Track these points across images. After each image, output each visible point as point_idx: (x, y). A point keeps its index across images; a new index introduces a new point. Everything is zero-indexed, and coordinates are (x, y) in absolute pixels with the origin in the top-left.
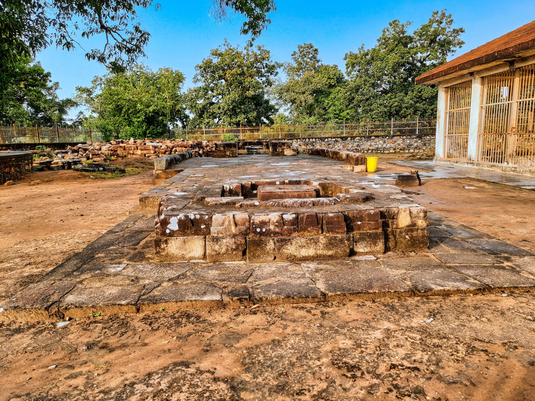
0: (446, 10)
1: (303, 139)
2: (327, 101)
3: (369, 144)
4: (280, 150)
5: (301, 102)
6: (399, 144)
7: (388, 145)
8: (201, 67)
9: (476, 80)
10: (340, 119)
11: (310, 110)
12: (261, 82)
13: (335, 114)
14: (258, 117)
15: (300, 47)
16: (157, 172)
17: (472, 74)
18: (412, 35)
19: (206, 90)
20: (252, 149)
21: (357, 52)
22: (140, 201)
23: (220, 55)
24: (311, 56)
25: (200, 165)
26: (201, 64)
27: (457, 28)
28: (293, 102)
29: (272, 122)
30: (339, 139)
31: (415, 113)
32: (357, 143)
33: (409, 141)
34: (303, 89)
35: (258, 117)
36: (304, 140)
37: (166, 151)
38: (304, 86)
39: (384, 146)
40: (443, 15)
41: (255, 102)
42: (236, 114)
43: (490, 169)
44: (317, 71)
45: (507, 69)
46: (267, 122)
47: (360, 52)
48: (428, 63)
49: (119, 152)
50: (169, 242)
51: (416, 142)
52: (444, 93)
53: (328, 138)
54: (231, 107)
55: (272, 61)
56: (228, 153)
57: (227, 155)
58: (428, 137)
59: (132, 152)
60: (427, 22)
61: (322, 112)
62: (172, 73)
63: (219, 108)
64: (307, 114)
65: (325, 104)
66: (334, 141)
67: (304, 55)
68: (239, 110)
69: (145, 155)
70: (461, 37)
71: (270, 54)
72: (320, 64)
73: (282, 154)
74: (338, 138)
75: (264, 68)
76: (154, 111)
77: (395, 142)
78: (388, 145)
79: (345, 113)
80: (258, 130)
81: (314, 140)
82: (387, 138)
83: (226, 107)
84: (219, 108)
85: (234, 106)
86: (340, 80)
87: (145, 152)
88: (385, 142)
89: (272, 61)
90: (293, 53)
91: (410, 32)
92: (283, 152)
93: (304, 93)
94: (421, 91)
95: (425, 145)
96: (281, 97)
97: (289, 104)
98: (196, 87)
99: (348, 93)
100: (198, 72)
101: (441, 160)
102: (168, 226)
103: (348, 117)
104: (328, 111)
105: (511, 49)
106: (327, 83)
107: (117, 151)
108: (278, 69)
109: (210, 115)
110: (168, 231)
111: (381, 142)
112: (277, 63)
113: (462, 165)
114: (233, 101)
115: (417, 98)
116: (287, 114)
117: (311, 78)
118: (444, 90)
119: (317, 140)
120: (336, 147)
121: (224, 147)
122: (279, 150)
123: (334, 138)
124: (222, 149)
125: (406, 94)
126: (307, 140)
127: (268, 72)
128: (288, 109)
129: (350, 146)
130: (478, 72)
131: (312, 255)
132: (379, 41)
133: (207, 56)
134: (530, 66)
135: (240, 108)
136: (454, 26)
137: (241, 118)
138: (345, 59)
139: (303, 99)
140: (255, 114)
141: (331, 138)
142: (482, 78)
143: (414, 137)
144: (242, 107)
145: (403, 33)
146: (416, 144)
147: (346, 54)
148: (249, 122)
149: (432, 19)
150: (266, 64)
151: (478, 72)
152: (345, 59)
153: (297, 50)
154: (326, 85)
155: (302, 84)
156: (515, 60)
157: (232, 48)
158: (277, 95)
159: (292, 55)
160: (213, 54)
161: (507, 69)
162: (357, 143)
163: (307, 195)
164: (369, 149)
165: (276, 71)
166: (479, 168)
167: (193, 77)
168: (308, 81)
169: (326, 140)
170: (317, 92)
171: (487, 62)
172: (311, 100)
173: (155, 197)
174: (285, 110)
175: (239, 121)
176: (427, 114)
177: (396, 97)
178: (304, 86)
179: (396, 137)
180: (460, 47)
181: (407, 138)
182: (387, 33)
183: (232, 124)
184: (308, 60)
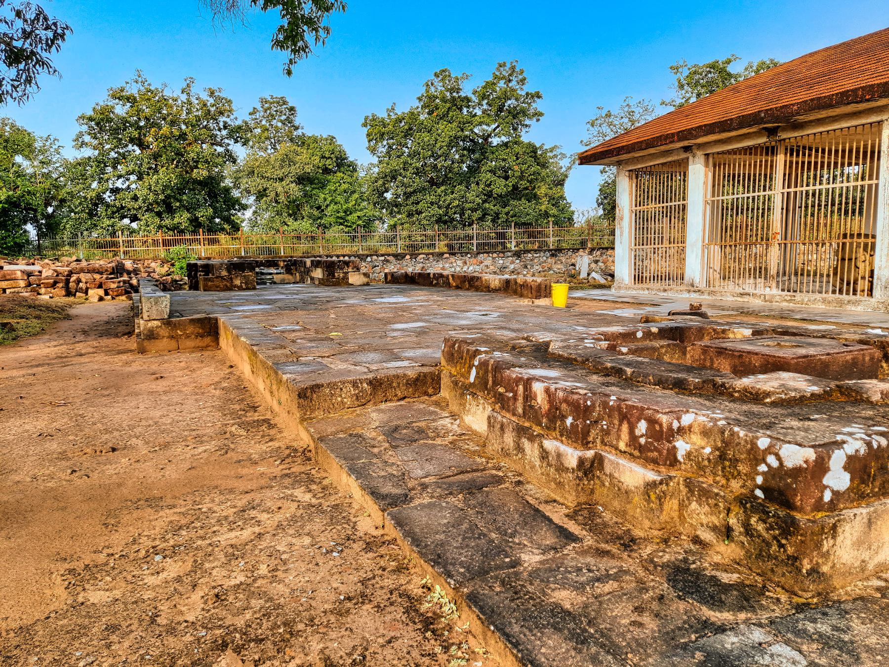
0: (517, 61)
2: (323, 196)
3: (441, 266)
5: (277, 195)
6: (487, 266)
7: (471, 268)
8: (91, 119)
9: (696, 159)
10: (347, 226)
11: (294, 209)
13: (338, 217)
15: (263, 101)
16: (150, 324)
17: (687, 149)
18: (470, 95)
19: (101, 163)
20: (262, 274)
21: (385, 115)
22: (300, 396)
23: (131, 100)
25: (493, 299)
26: (90, 113)
27: (532, 91)
30: (391, 258)
31: (482, 219)
32: (421, 265)
33: (501, 262)
37: (55, 283)
40: (513, 68)
42: (170, 210)
43: (739, 299)
44: (302, 142)
45: (762, 140)
47: (389, 115)
48: (495, 141)
50: (840, 530)
51: (513, 262)
52: (627, 179)
54: (161, 197)
55: (236, 119)
56: (237, 282)
57: (235, 286)
58: (530, 255)
60: (490, 79)
61: (316, 213)
63: (135, 198)
64: (290, 215)
65: (321, 200)
66: (383, 261)
70: (538, 105)
73: (344, 282)
74: (389, 255)
77: (482, 263)
78: (471, 268)
79: (355, 215)
82: (469, 256)
85: (168, 197)
86: (342, 162)
88: (465, 263)
89: (236, 119)
90: (252, 110)
91: (467, 90)
92: (345, 278)
93: (281, 180)
94: (490, 185)
95: (526, 267)
98: (79, 157)
99: (380, 182)
101: (628, 288)
102: (825, 481)
103: (360, 222)
104: (325, 212)
105: (795, 107)
109: (113, 213)
110: (827, 496)
111: (460, 263)
113: (676, 295)
114: (166, 187)
115: (485, 195)
117: (291, 156)
118: (627, 174)
121: (229, 270)
122: (339, 274)
124: (224, 273)
127: (230, 136)
130: (700, 146)
132: (420, 99)
133: (103, 99)
134: (812, 137)
135: (180, 201)
136: (529, 88)
137: (182, 218)
138: (365, 125)
139: (280, 189)
142: (707, 155)
143: (509, 254)
145: (458, 90)
146: (512, 267)
147: (366, 118)
149: (498, 73)
150: (225, 123)
151: (700, 146)
152: (365, 125)
153: (258, 106)
154: (318, 168)
155: (278, 164)
156: (779, 127)
159: (250, 114)
160: (114, 97)
161: (762, 140)
162: (421, 265)
166: (714, 297)
167: (74, 137)
168: (288, 160)
169: (369, 259)
171: (741, 126)
172: (295, 190)
173: (335, 384)
176: (500, 221)
177: (452, 193)
180: (538, 120)
181: (499, 257)
182: (433, 89)
184: (280, 124)
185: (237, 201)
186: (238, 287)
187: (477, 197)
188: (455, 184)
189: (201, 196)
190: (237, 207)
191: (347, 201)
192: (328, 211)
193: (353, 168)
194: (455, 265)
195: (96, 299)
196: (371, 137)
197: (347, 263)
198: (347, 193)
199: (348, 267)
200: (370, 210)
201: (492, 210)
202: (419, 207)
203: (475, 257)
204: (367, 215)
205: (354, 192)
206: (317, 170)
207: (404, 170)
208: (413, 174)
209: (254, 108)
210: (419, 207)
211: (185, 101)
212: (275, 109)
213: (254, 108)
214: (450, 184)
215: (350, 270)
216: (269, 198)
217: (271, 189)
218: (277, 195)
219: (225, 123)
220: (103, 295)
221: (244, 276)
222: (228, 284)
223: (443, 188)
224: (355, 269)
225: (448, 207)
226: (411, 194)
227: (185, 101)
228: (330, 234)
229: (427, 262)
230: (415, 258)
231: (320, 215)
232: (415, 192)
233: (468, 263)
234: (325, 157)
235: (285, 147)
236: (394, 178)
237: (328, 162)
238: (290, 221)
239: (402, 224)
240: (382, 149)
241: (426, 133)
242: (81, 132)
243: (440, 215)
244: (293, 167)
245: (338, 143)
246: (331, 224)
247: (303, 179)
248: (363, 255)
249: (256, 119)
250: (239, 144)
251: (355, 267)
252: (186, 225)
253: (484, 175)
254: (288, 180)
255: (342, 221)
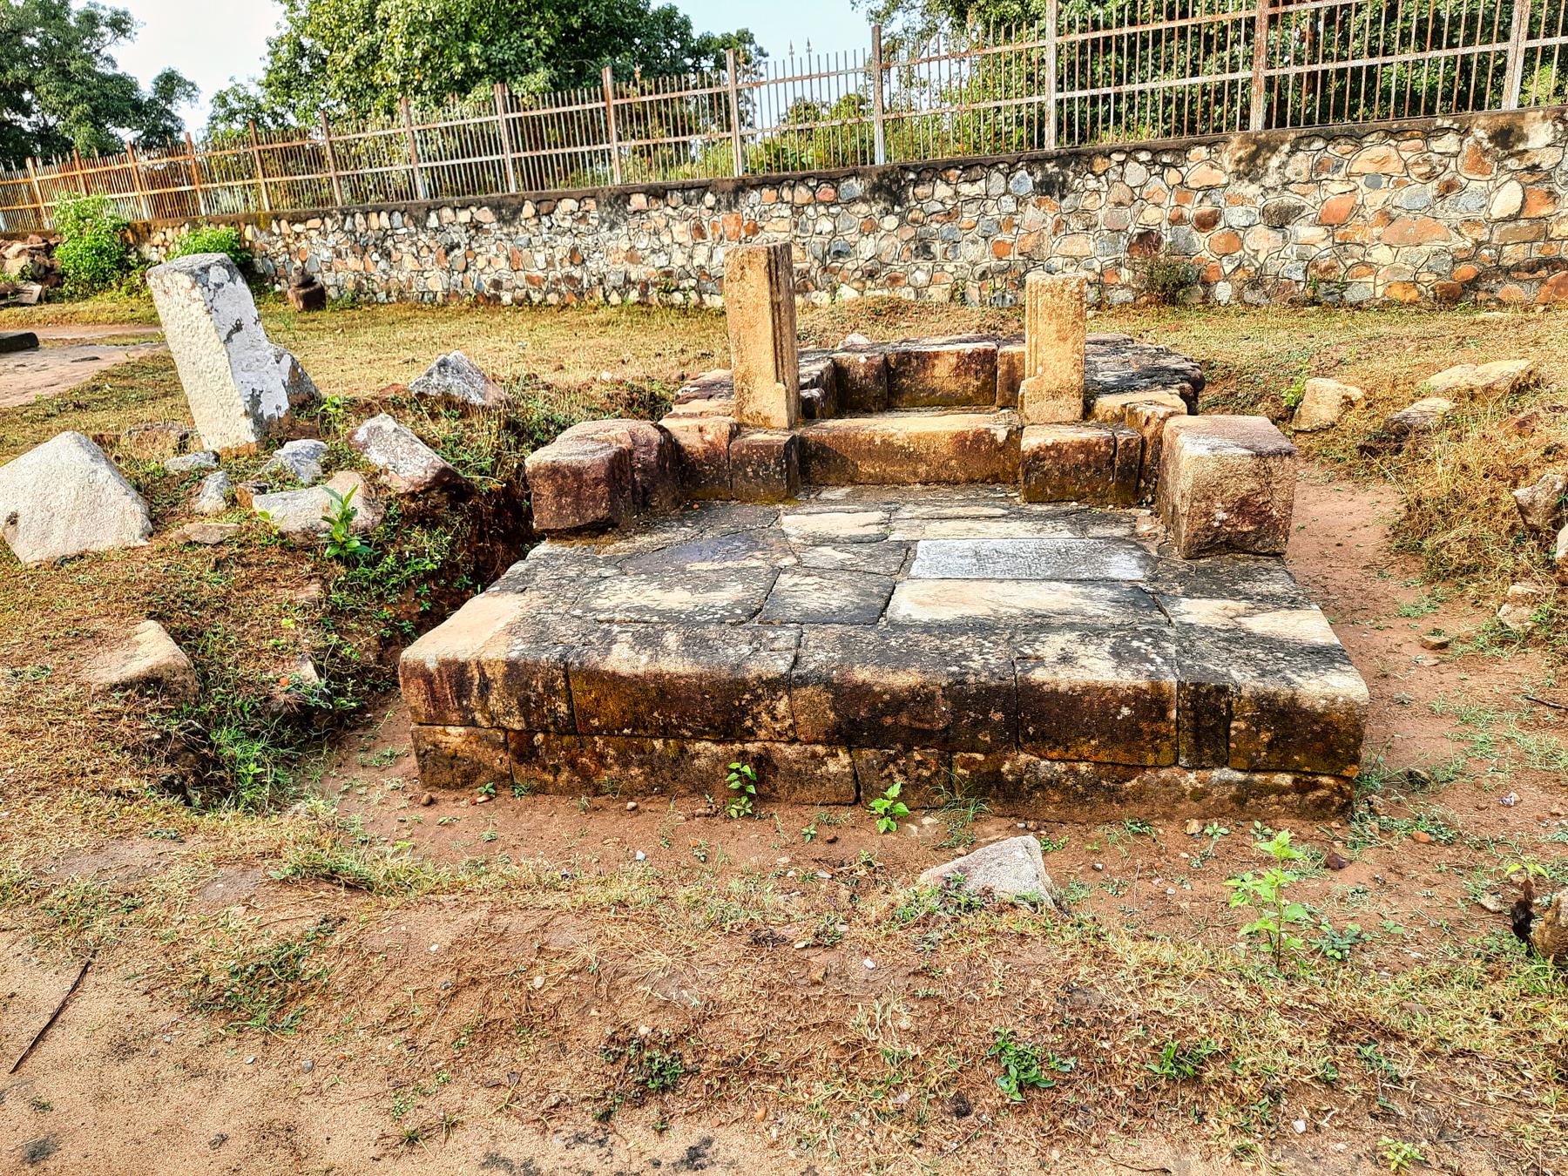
33: (826, 225)
51: (870, 228)
58: (942, 190)
62: (129, 126)
88: (699, 231)
95: (924, 249)
131: (624, 674)
146: (867, 247)
163: (408, 626)
179: (754, 196)
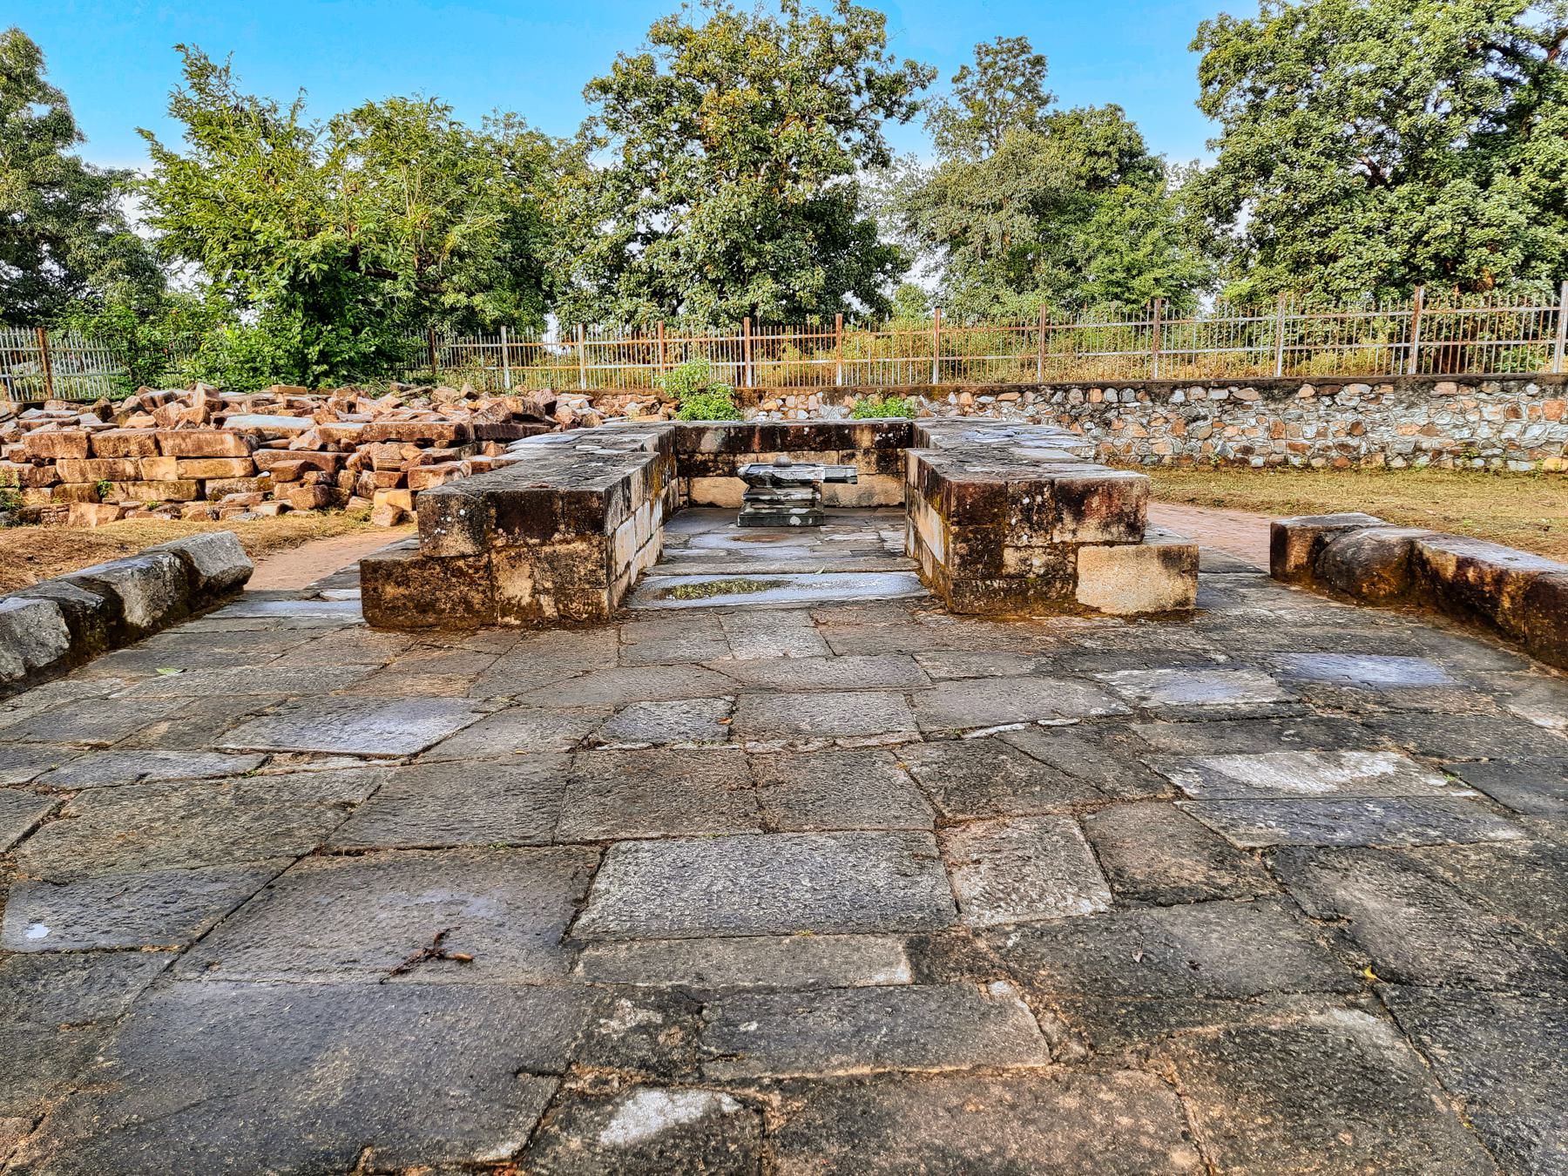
1: (1055, 388)
2: (1083, 237)
4: (1038, 561)
5: (987, 240)
8: (604, 88)
10: (1128, 301)
11: (1019, 269)
12: (846, 147)
13: (1111, 283)
14: (831, 291)
15: (983, 51)
20: (777, 483)
24: (1019, 81)
26: (607, 74)
28: (956, 240)
29: (882, 309)
30: (1250, 395)
34: (996, 194)
35: (831, 291)
36: (1059, 396)
38: (1001, 179)
39: (1512, 432)
41: (821, 230)
42: (741, 278)
44: (1057, 128)
46: (866, 310)
49: (61, 468)
53: (1186, 385)
54: (721, 247)
55: (891, 59)
56: (518, 586)
57: (508, 607)
59: (130, 469)
61: (1064, 275)
63: (676, 254)
64: (1009, 282)
66: (1222, 403)
67: (997, 79)
68: (753, 262)
69: (201, 483)
71: (887, 29)
72: (1049, 110)
74: (1243, 385)
75: (858, 93)
76: (326, 254)
78: (1536, 430)
79: (1148, 277)
80: (829, 344)
81: (1111, 395)
82: (1532, 388)
83: (701, 248)
84: (676, 254)
85: (735, 248)
87: (198, 468)
89: (891, 59)
90: (957, 73)
93: (998, 207)
96: (915, 225)
97: (942, 251)
99: (1226, 182)
100: (598, 109)
106: (1083, 170)
107: (52, 461)
108: (917, 90)
112: (913, 67)
114: (729, 224)
115: (1535, 202)
116: (931, 284)
119: (1128, 394)
120: (1229, 432)
121: (476, 527)
123: (1223, 386)
125: (1485, 185)
126: (1076, 395)
127: (878, 103)
128: (936, 269)
129: (1310, 431)
133: (636, 44)
135: (758, 254)
137: (762, 291)
139: (994, 228)
140: (819, 276)
141: (1206, 386)
144: (769, 246)
147: (1203, 27)
148: (796, 312)
150: (870, 73)
153: (972, 63)
154: (1079, 177)
157: (733, 14)
158: (898, 218)
162: (1350, 417)
164: (1418, 449)
165: (906, 99)
167: (578, 130)
168: (1015, 163)
169: (1178, 396)
170: (1043, 206)
172: (1024, 227)
174: (926, 274)
175: (754, 307)
178: (1001, 179)
183: (724, 318)
184: (1010, 96)
185: (889, 252)
186: (521, 611)
187: (1512, 207)
188: (1442, 176)
189: (805, 242)
190: (889, 267)
191: (1134, 246)
192: (1091, 271)
193: (1154, 172)
194: (1472, 418)
195: (387, 517)
196: (1211, 75)
197: (1073, 499)
198: (1136, 229)
199: (1079, 516)
200: (1186, 260)
201: (1554, 244)
202: (1330, 244)
203: (1555, 394)
204: (1177, 275)
205: (1152, 225)
206: (1075, 182)
207: (1296, 145)
208: (1321, 153)
209: (963, 68)
210: (1330, 244)
211: (787, 27)
212: (1003, 64)
213: (963, 68)
214: (1426, 177)
215: (1083, 535)
216: (971, 248)
217: (975, 229)
218: (987, 240)
219: (870, 73)
220: (408, 508)
221: (552, 559)
222: (476, 598)
223: (1404, 189)
224: (1117, 530)
225: (1417, 239)
226: (1311, 209)
227: (787, 27)
228: (1089, 321)
229: (1372, 406)
230: (1332, 396)
231: (1072, 279)
232: (1322, 202)
233: (1525, 412)
234: (1095, 153)
235: (1013, 137)
236: (1265, 170)
237: (1102, 162)
238: (1008, 294)
239: (1274, 291)
240: (1237, 102)
241: (1371, 40)
242: (591, 118)
243: (1391, 262)
244: (1025, 179)
245: (1127, 119)
246: (1093, 298)
247: (1045, 205)
248: (1162, 385)
249: (965, 90)
250: (894, 120)
251: (1119, 517)
252: (767, 307)
253: (1542, 144)
254: (1010, 208)
255: (1118, 290)
